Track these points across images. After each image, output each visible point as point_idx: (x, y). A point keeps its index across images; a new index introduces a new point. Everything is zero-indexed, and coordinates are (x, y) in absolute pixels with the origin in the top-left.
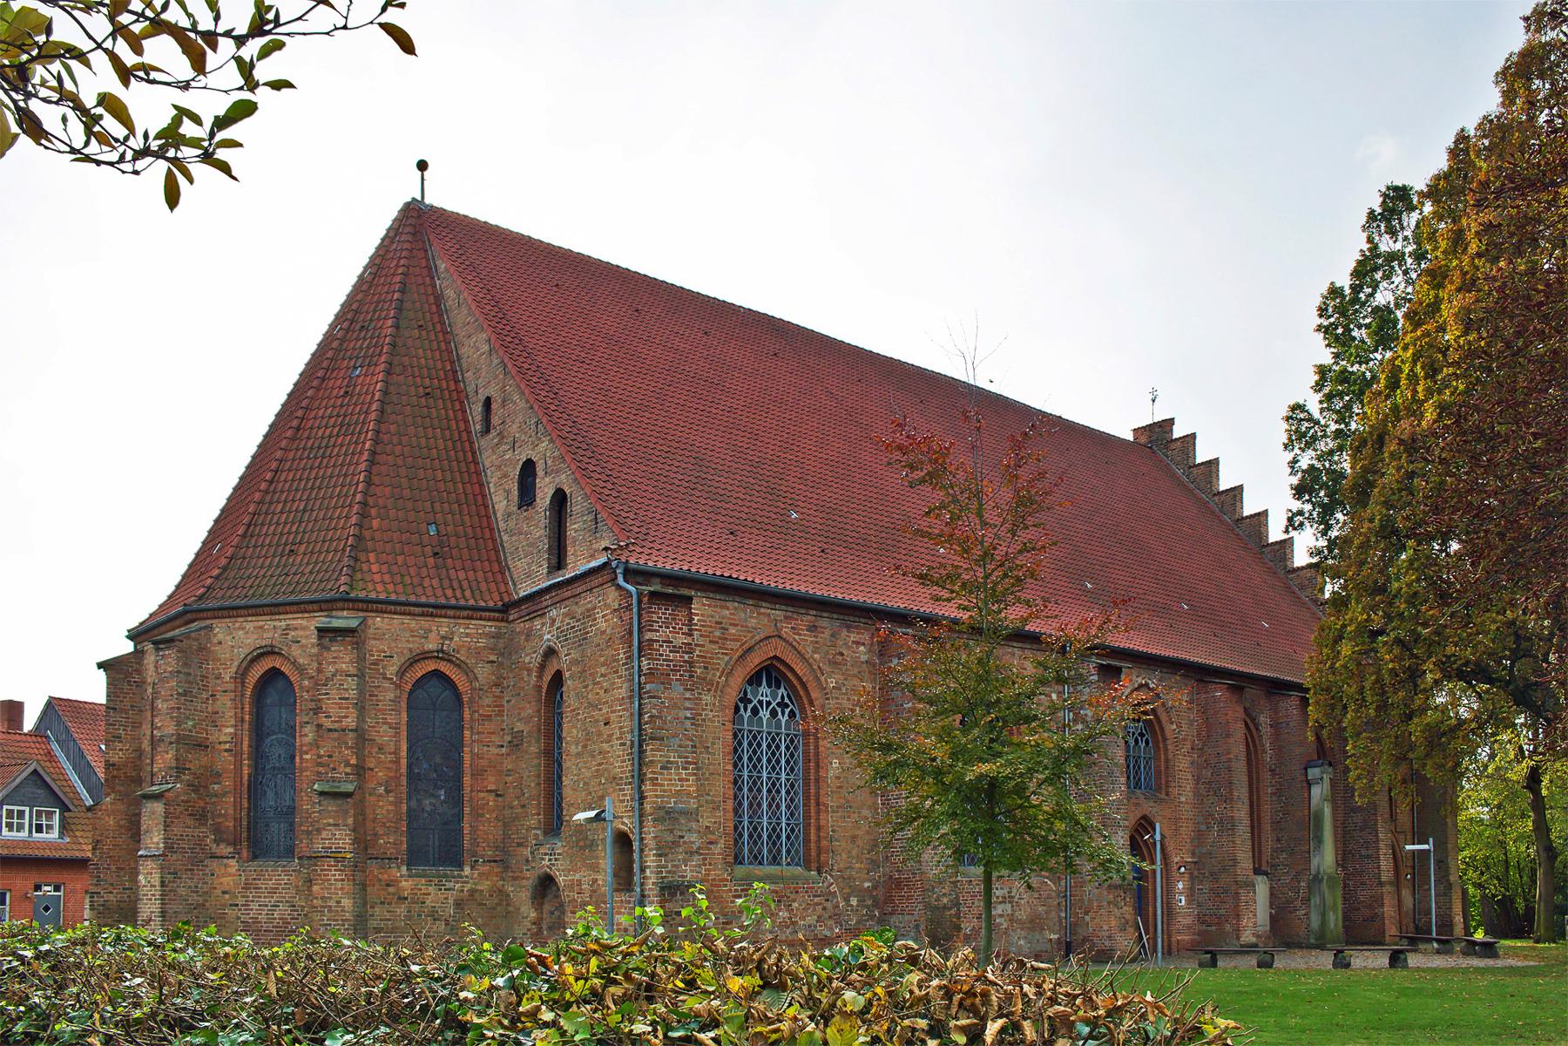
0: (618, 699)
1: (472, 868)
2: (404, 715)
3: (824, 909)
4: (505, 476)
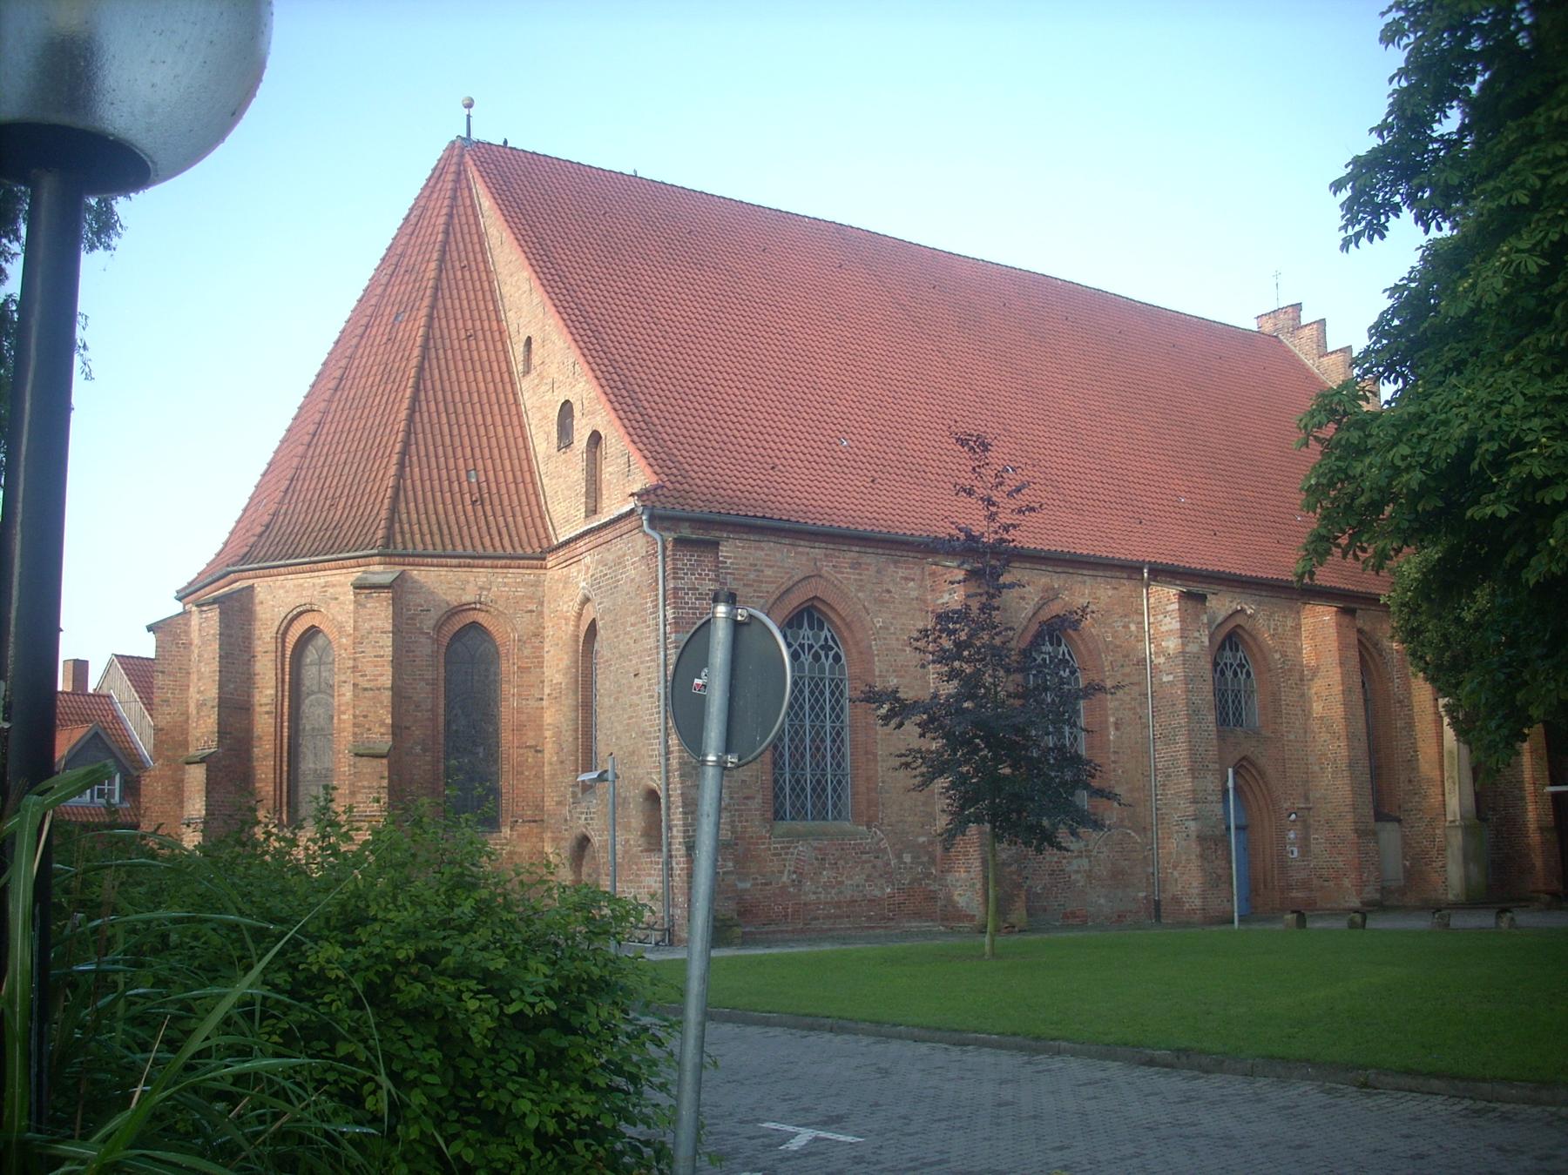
0: (646, 650)
1: (512, 829)
2: (442, 670)
3: (874, 867)
4: (545, 417)
